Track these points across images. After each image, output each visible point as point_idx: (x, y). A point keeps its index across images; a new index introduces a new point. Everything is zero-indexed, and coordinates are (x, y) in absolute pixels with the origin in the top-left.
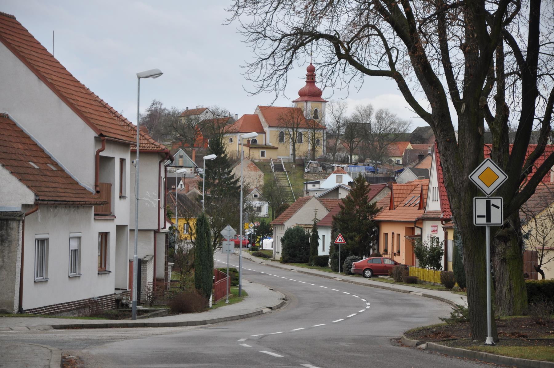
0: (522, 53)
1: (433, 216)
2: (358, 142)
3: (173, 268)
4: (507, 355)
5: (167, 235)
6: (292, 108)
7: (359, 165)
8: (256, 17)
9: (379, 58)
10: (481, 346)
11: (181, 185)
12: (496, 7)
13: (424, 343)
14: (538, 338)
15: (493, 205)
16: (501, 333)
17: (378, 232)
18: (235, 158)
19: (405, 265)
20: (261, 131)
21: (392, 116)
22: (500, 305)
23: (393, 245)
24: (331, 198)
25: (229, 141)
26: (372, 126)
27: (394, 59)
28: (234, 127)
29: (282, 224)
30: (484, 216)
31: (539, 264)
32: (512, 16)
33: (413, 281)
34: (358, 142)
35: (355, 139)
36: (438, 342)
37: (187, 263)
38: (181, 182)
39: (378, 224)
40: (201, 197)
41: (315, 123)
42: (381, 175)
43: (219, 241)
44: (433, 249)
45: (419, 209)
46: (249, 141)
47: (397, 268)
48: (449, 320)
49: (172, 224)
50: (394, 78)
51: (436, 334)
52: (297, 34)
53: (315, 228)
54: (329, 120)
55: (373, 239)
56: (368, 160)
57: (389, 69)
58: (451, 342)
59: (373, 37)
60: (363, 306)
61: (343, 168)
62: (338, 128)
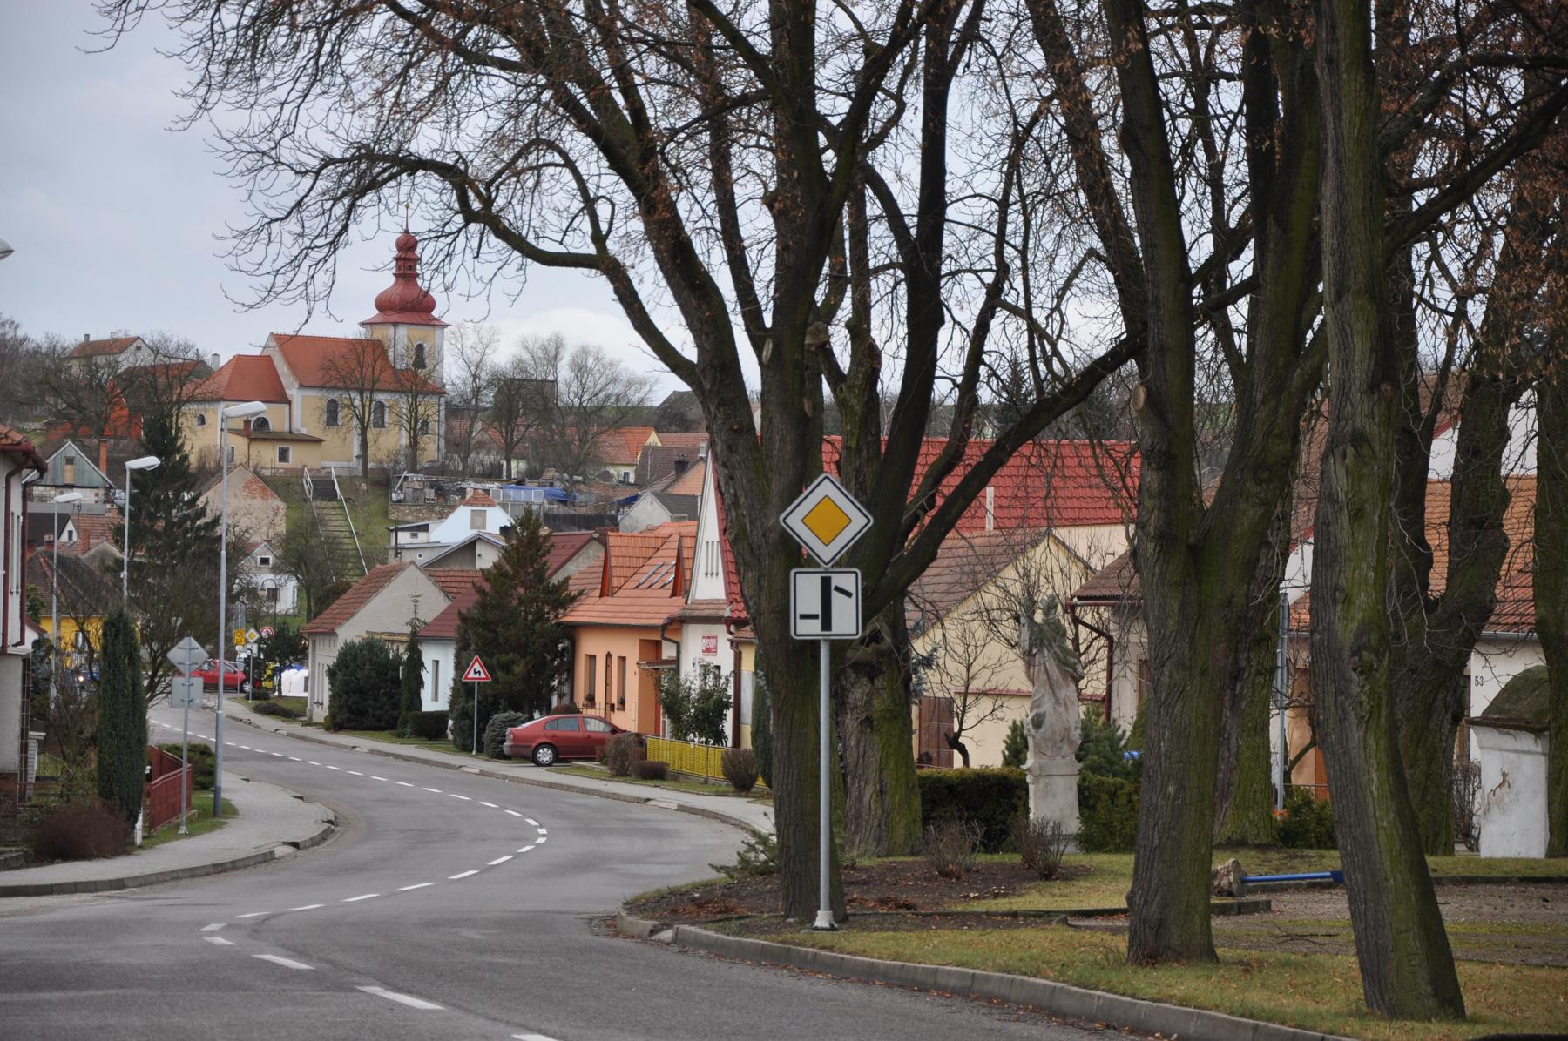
0: (907, 220)
1: (706, 612)
2: (527, 428)
3: (44, 746)
4: (864, 953)
5: (26, 661)
6: (360, 342)
7: (529, 484)
8: (255, 114)
9: (565, 224)
10: (803, 934)
11: (70, 533)
12: (844, 105)
13: (669, 926)
14: (941, 910)
15: (838, 589)
16: (853, 900)
17: (572, 650)
18: (211, 464)
19: (638, 735)
20: (279, 397)
21: (611, 364)
22: (856, 832)
23: (608, 684)
24: (455, 567)
25: (195, 421)
26: (561, 387)
27: (604, 227)
28: (210, 386)
29: (332, 633)
30: (815, 617)
31: (956, 730)
32: (885, 133)
33: (656, 773)
34: (527, 428)
35: (519, 421)
36: (703, 924)
37: (81, 732)
38: (70, 526)
39: (572, 632)
40: (119, 562)
41: (416, 380)
42: (583, 511)
43: (165, 675)
44: (705, 695)
45: (674, 594)
46: (247, 423)
47: (618, 742)
48: (735, 869)
49: (41, 632)
50: (605, 272)
51: (700, 906)
52: (360, 158)
53: (415, 642)
54: (452, 372)
55: (558, 670)
56: (551, 473)
57: (591, 249)
58: (735, 924)
59: (551, 170)
60: (527, 836)
61: (487, 491)
62: (477, 392)
